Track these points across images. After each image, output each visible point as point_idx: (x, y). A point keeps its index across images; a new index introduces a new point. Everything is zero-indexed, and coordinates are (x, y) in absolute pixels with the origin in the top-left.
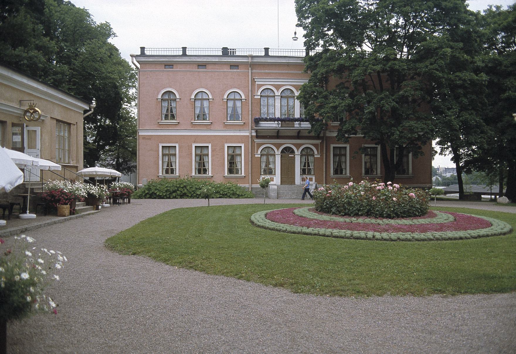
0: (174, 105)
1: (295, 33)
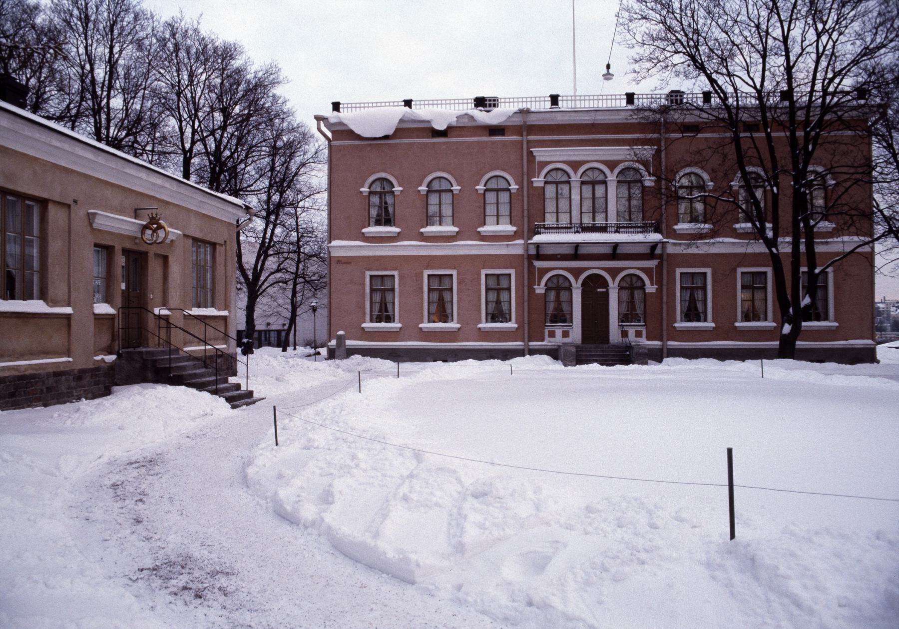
1: (608, 66)
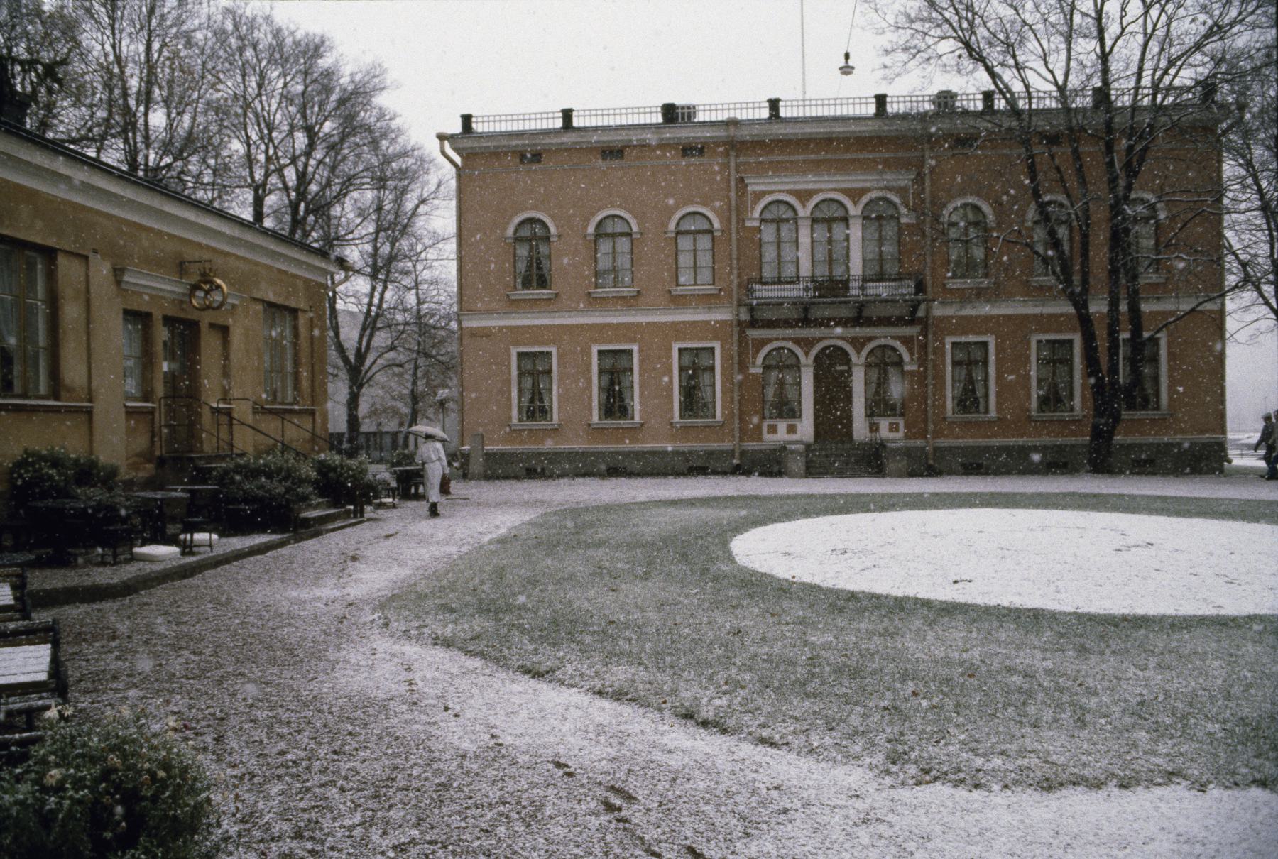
0: (543, 249)
1: (847, 56)
